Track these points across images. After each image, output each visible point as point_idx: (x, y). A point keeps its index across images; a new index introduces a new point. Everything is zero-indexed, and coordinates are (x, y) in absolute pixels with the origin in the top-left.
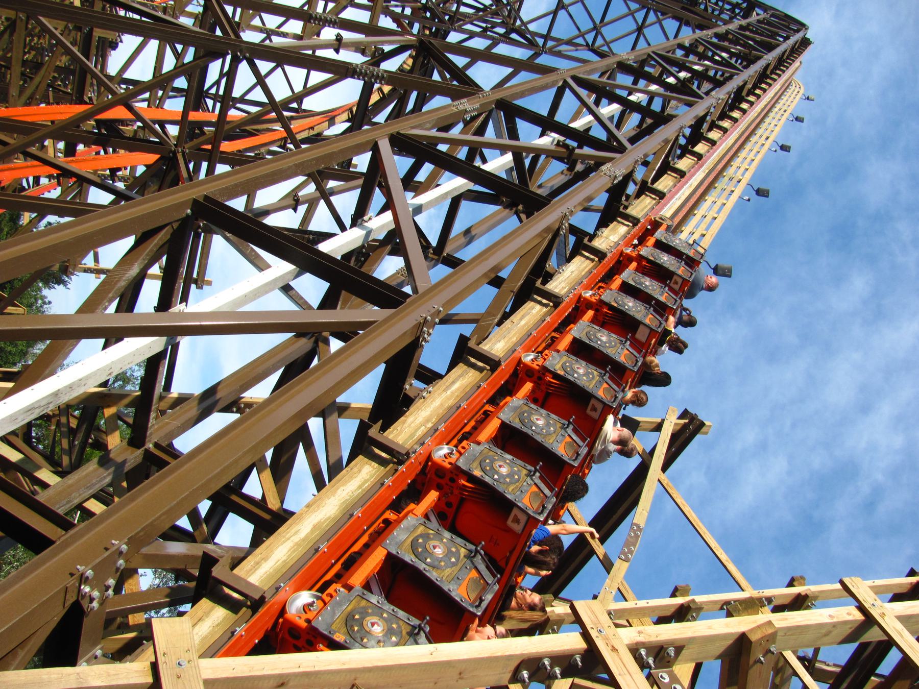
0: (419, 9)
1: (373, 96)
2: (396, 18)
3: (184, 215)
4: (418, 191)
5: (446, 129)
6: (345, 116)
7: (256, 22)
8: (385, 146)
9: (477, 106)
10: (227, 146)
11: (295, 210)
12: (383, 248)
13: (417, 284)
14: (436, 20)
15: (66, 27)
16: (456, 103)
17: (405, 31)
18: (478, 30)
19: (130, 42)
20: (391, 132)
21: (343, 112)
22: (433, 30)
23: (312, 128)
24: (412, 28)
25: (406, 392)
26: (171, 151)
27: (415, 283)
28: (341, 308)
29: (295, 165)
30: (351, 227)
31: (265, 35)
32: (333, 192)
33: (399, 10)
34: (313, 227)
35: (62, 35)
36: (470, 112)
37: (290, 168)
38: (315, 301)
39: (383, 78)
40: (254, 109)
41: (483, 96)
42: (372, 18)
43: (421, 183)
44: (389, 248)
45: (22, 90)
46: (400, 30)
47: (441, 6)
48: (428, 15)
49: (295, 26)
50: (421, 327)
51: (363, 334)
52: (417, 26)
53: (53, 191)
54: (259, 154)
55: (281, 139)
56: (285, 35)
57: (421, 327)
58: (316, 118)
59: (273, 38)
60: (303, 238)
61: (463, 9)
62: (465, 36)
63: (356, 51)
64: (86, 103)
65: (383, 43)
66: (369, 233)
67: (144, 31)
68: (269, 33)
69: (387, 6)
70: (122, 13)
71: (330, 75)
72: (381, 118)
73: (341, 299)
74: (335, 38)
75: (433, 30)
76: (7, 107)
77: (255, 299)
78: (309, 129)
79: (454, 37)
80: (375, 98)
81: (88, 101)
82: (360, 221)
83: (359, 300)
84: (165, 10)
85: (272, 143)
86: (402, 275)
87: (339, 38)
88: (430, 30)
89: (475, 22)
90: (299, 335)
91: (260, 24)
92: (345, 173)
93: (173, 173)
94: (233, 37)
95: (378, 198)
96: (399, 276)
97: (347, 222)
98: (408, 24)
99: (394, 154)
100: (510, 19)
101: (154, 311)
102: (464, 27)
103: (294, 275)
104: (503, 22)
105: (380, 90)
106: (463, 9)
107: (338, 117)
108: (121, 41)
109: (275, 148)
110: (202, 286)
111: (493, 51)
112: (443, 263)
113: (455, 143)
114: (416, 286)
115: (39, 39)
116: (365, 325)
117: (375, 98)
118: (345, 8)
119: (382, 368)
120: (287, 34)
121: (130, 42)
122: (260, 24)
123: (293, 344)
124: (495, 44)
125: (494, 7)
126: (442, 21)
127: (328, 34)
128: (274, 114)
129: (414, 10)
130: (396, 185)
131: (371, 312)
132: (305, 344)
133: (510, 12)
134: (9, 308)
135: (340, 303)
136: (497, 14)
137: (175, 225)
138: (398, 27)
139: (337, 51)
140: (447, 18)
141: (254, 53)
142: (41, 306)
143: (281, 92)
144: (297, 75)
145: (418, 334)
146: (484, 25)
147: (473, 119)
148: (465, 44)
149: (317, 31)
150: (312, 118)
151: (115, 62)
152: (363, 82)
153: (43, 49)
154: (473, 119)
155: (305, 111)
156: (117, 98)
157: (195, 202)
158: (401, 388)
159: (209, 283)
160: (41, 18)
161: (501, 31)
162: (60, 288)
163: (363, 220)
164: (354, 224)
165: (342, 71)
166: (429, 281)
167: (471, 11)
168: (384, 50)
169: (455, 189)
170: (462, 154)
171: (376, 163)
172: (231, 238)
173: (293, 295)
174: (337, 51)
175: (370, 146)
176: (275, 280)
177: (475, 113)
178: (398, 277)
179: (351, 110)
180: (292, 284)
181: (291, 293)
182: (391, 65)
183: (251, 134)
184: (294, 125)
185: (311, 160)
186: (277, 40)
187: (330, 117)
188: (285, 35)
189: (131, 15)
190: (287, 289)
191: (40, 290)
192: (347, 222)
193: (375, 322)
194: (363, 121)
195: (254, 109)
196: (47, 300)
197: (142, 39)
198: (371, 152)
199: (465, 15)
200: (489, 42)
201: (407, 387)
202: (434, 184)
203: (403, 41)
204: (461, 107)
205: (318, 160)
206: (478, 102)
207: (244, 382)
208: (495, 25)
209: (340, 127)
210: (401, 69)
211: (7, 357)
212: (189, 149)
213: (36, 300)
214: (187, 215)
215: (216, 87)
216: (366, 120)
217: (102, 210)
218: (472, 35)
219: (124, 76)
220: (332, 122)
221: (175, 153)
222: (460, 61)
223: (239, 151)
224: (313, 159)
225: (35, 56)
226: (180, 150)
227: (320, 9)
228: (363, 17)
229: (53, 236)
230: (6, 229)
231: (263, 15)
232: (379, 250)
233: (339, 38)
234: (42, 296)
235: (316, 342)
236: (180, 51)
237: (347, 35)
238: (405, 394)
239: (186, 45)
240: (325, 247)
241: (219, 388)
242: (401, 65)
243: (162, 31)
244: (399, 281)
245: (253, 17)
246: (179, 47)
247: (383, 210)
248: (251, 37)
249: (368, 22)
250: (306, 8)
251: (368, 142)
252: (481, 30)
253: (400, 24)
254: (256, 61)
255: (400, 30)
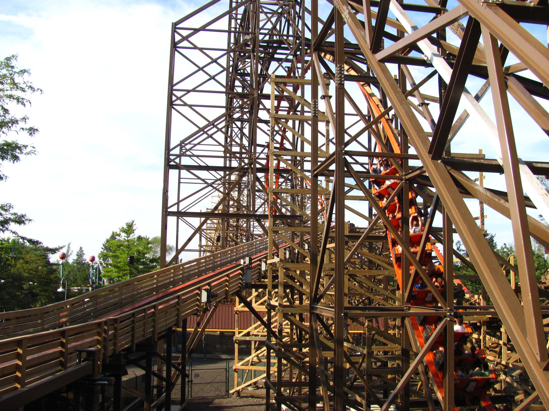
0: (297, 59)
1: (352, 74)
2: (305, 71)
3: (442, 164)
4: (404, 31)
5: (363, 23)
6: (367, 88)
7: (324, 148)
8: (380, 55)
9: (345, 7)
10: (397, 150)
11: (428, 104)
12: (443, 45)
13: (461, 14)
14: (301, 47)
15: (347, 249)
16: (346, 20)
17: (312, 64)
18: (300, 21)
19: (349, 217)
20: (371, 54)
21: (365, 89)
22: (306, 48)
23: (378, 106)
24: (308, 61)
25: (536, 4)
26: (406, 182)
27: (461, 15)
28: (486, 63)
29: (401, 105)
30: (433, 66)
31: (330, 143)
32: (414, 84)
33: (300, 71)
34: (436, 93)
35: (350, 251)
36: (349, 10)
37: (403, 108)
38: (482, 81)
39: (341, 70)
40: (373, 140)
41: (338, 5)
42: (308, 84)
43: (398, 31)
44: (442, 42)
45: (385, 269)
46: (311, 68)
47: (292, 46)
48: (298, 53)
49: (322, 126)
50: (490, 4)
51: (500, 40)
52: (307, 58)
53: (439, 249)
54: (399, 134)
55: (388, 123)
56: (328, 131)
57: (490, 4)
58: (371, 105)
59: (330, 138)
60: (444, 96)
61: (291, 33)
62: (306, 29)
63: (329, 89)
64: (386, 234)
65: (320, 72)
66: (435, 55)
67: (341, 209)
68: (329, 140)
69: (299, 77)
70: (333, 224)
71: (345, 98)
72: (364, 67)
73: (479, 64)
74: (323, 100)
75: (306, 48)
76: (396, 276)
77: (487, 116)
78: (378, 107)
79: (308, 35)
80: (353, 73)
81: (385, 234)
82: (428, 62)
83: (476, 52)
84: (327, 199)
85: (391, 128)
86: (457, 30)
87: (323, 97)
88: (307, 50)
89: (297, 24)
90: (507, 87)
91: (325, 146)
92: (402, 77)
93: (418, 179)
94: (335, 156)
95: (414, 54)
96: (458, 32)
97: (430, 70)
98: (307, 64)
99: (383, 49)
100: (289, 4)
101: (504, 174)
102: (301, 30)
103: (467, 94)
104: (293, 8)
105: (347, 71)
106: (291, 33)
107: (368, 92)
108: (349, 222)
109: (393, 125)
110: (483, 155)
111: (310, 9)
112: (445, 7)
113: (369, 15)
114: (463, 14)
115: (356, 264)
116: (494, 41)
117: (353, 73)
118: (305, 100)
119: (521, 24)
120: (327, 130)
121: (349, 217)
122: (325, 146)
123: (512, 89)
124: (306, 9)
125: (285, 16)
126: (300, 44)
127: (322, 106)
128: (373, 126)
129: (299, 62)
130: (401, 43)
131: (483, 42)
132: (511, 82)
133: (286, 6)
134: (511, 263)
135: (481, 65)
136: (289, 12)
137: (449, 168)
138: (309, 69)
139: (330, 97)
140: (298, 41)
141: (341, 143)
142: (508, 249)
143: (362, 125)
144: (348, 121)
145: (494, 5)
146: (297, 19)
147: (353, 8)
148: (310, 28)
149: (322, 114)
150: (372, 107)
151: (362, 224)
152: (345, 82)
153: (361, 262)
154: (353, 8)
155: (369, 112)
156: (381, 216)
157: (433, 159)
158: (534, 8)
159: (480, 151)
160: (345, 260)
161: (298, 8)
162: (495, 239)
163: (427, 60)
164: (431, 65)
165: (341, 92)
166: (459, 6)
167: (291, 29)
168: (324, 73)
169: (398, 9)
170: (375, 10)
171: (391, 59)
172: (451, 135)
173: (481, 93)
174: (330, 97)
175: (382, 64)
176: (474, 105)
177: (349, 7)
178: (459, 32)
179: (363, 85)
180: (474, 95)
181: (480, 95)
182: (333, 67)
183: (388, 140)
184: (376, 115)
185: (397, 97)
186: (332, 135)
187: (369, 97)
188: (328, 131)
189: (334, 212)
190: (478, 98)
191: (498, 250)
192: (430, 70)
193: (491, 35)
194: (367, 77)
195: (373, 140)
196: (504, 246)
197: (345, 209)
198: (386, 64)
199: (294, 31)
200: (306, 14)
201: (532, 4)
202: (397, 22)
203: (317, 61)
204: (348, 16)
205: (396, 93)
206: (342, 7)
207: (541, 115)
208: (296, 12)
209: (374, 90)
210: (333, 61)
211: (541, 266)
212: (402, 173)
213: (504, 252)
214: (442, 162)
215: (364, 165)
216: (367, 75)
217: (446, 210)
218: (304, 24)
219: (368, 216)
220: (372, 95)
221: (406, 180)
222: (320, 26)
223: (399, 145)
224: (396, 95)
225: (366, 266)
226: (404, 177)
227: (309, 115)
228: (308, 89)
229: (465, 236)
230: (464, 272)
231: (319, 146)
232: (445, 48)
233: (323, 97)
234: (502, 249)
235: (509, 75)
236: (349, 188)
237: (321, 93)
238: (538, 4)
239: (344, 185)
240: (447, 79)
241: (546, 129)
242: (331, 61)
243: (339, 196)
244: (461, 31)
245: (322, 151)
246: (346, 189)
247: (419, 51)
248: (332, 149)
249: (311, 86)
250: (310, 122)
251: (380, 66)
252: (300, 20)
253: (308, 68)
254: (345, 141)
255: (311, 68)
